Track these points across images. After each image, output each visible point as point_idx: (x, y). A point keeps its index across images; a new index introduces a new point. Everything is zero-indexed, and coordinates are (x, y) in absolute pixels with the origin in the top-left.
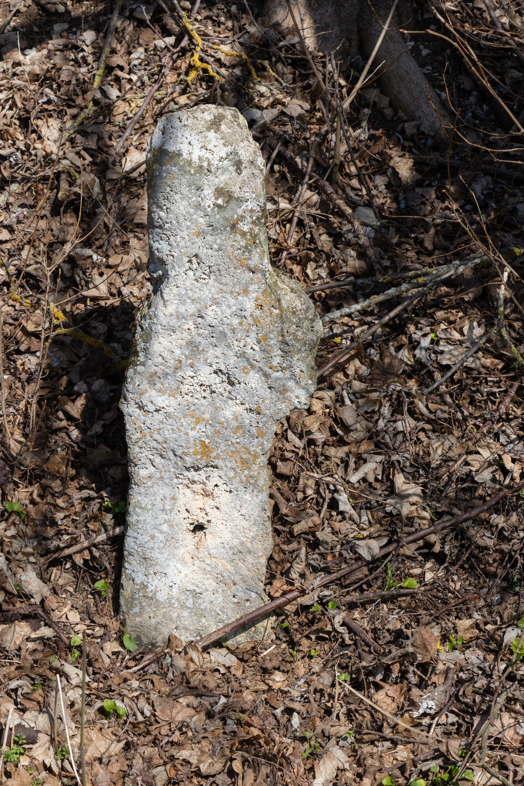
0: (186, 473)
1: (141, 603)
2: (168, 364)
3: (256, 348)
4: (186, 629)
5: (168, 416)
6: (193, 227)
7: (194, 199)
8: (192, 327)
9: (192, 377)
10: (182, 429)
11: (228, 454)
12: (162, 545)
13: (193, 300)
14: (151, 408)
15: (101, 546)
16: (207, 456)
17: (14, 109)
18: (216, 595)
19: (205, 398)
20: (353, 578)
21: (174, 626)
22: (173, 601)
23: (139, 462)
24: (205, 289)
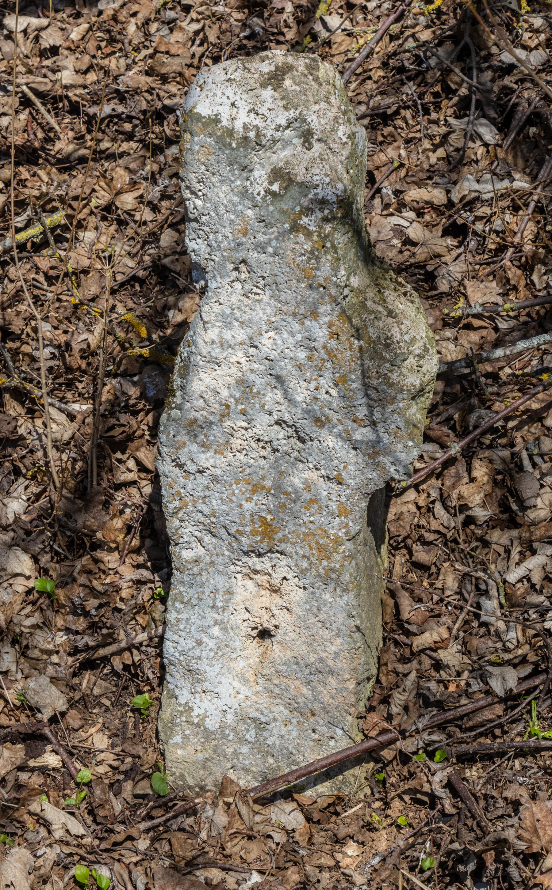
0: (245, 559)
1: (183, 730)
2: (212, 410)
3: (333, 392)
4: (247, 771)
5: (215, 479)
6: (237, 221)
7: (239, 183)
8: (243, 361)
9: (246, 429)
10: (234, 498)
11: (298, 536)
12: (212, 654)
13: (242, 323)
14: (192, 468)
15: (144, 648)
16: (270, 538)
17: (206, 45)
18: (290, 727)
19: (265, 458)
20: (479, 718)
21: (229, 765)
22: (227, 732)
23: (181, 541)
24: (258, 308)
